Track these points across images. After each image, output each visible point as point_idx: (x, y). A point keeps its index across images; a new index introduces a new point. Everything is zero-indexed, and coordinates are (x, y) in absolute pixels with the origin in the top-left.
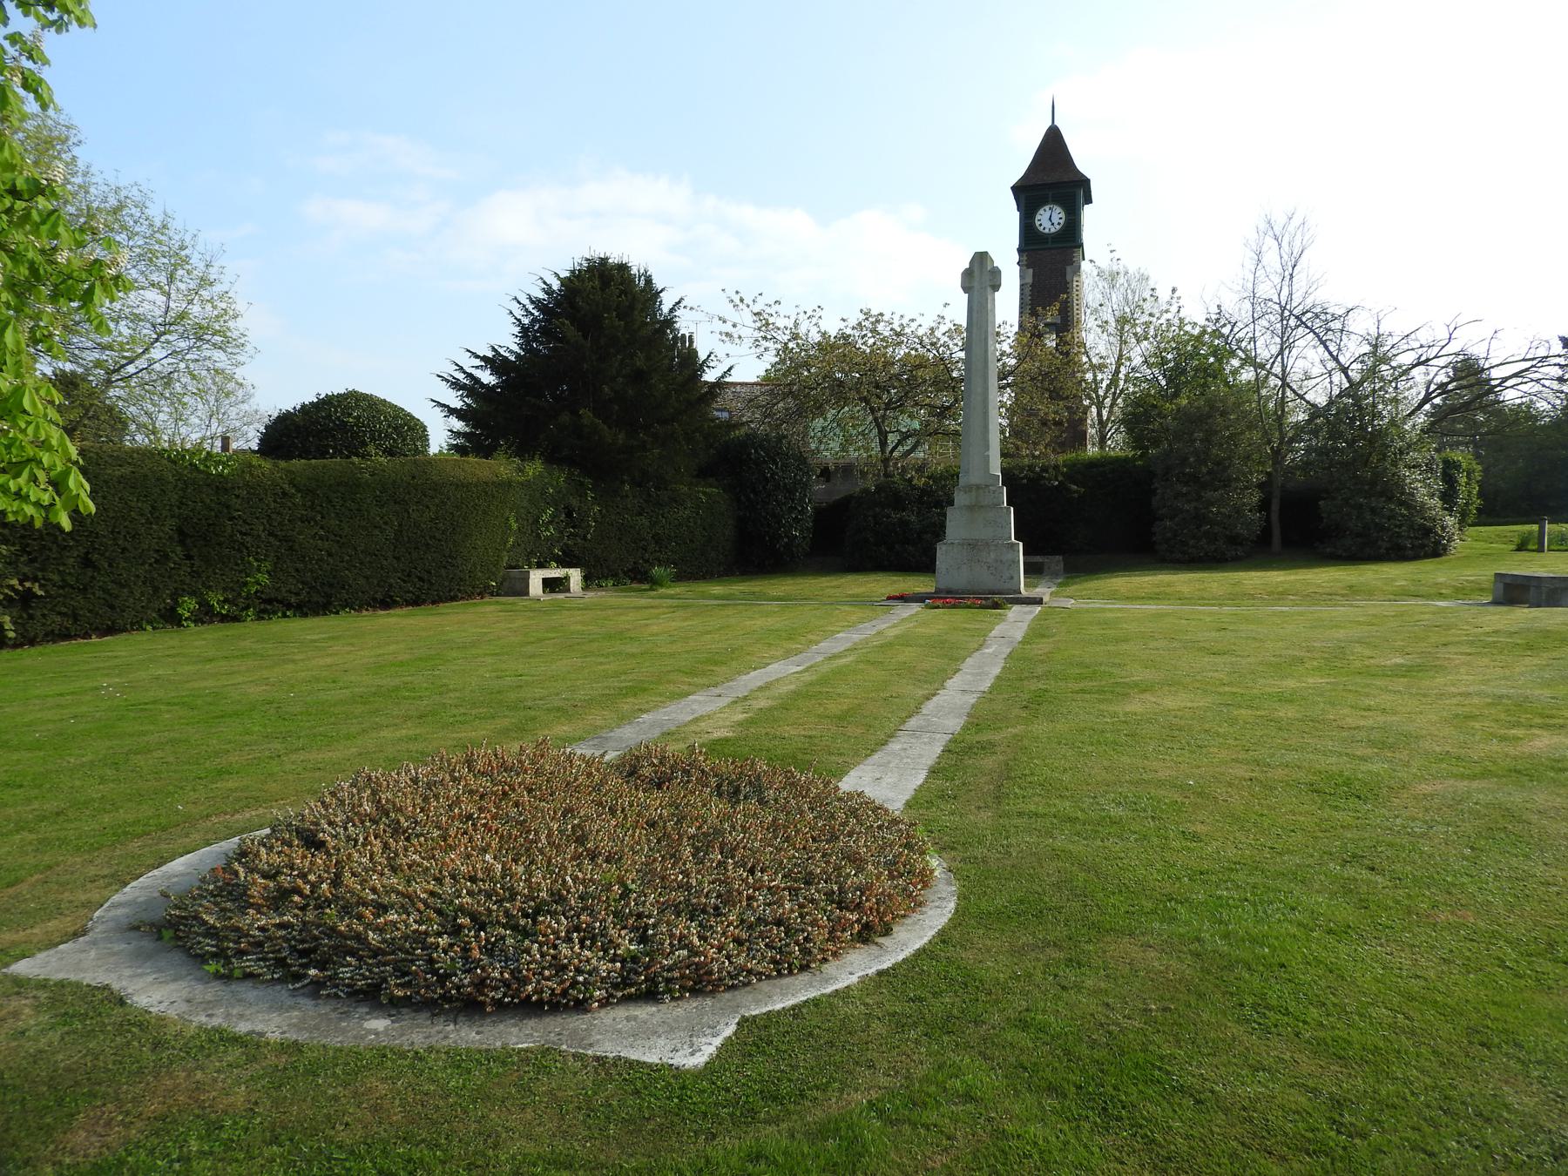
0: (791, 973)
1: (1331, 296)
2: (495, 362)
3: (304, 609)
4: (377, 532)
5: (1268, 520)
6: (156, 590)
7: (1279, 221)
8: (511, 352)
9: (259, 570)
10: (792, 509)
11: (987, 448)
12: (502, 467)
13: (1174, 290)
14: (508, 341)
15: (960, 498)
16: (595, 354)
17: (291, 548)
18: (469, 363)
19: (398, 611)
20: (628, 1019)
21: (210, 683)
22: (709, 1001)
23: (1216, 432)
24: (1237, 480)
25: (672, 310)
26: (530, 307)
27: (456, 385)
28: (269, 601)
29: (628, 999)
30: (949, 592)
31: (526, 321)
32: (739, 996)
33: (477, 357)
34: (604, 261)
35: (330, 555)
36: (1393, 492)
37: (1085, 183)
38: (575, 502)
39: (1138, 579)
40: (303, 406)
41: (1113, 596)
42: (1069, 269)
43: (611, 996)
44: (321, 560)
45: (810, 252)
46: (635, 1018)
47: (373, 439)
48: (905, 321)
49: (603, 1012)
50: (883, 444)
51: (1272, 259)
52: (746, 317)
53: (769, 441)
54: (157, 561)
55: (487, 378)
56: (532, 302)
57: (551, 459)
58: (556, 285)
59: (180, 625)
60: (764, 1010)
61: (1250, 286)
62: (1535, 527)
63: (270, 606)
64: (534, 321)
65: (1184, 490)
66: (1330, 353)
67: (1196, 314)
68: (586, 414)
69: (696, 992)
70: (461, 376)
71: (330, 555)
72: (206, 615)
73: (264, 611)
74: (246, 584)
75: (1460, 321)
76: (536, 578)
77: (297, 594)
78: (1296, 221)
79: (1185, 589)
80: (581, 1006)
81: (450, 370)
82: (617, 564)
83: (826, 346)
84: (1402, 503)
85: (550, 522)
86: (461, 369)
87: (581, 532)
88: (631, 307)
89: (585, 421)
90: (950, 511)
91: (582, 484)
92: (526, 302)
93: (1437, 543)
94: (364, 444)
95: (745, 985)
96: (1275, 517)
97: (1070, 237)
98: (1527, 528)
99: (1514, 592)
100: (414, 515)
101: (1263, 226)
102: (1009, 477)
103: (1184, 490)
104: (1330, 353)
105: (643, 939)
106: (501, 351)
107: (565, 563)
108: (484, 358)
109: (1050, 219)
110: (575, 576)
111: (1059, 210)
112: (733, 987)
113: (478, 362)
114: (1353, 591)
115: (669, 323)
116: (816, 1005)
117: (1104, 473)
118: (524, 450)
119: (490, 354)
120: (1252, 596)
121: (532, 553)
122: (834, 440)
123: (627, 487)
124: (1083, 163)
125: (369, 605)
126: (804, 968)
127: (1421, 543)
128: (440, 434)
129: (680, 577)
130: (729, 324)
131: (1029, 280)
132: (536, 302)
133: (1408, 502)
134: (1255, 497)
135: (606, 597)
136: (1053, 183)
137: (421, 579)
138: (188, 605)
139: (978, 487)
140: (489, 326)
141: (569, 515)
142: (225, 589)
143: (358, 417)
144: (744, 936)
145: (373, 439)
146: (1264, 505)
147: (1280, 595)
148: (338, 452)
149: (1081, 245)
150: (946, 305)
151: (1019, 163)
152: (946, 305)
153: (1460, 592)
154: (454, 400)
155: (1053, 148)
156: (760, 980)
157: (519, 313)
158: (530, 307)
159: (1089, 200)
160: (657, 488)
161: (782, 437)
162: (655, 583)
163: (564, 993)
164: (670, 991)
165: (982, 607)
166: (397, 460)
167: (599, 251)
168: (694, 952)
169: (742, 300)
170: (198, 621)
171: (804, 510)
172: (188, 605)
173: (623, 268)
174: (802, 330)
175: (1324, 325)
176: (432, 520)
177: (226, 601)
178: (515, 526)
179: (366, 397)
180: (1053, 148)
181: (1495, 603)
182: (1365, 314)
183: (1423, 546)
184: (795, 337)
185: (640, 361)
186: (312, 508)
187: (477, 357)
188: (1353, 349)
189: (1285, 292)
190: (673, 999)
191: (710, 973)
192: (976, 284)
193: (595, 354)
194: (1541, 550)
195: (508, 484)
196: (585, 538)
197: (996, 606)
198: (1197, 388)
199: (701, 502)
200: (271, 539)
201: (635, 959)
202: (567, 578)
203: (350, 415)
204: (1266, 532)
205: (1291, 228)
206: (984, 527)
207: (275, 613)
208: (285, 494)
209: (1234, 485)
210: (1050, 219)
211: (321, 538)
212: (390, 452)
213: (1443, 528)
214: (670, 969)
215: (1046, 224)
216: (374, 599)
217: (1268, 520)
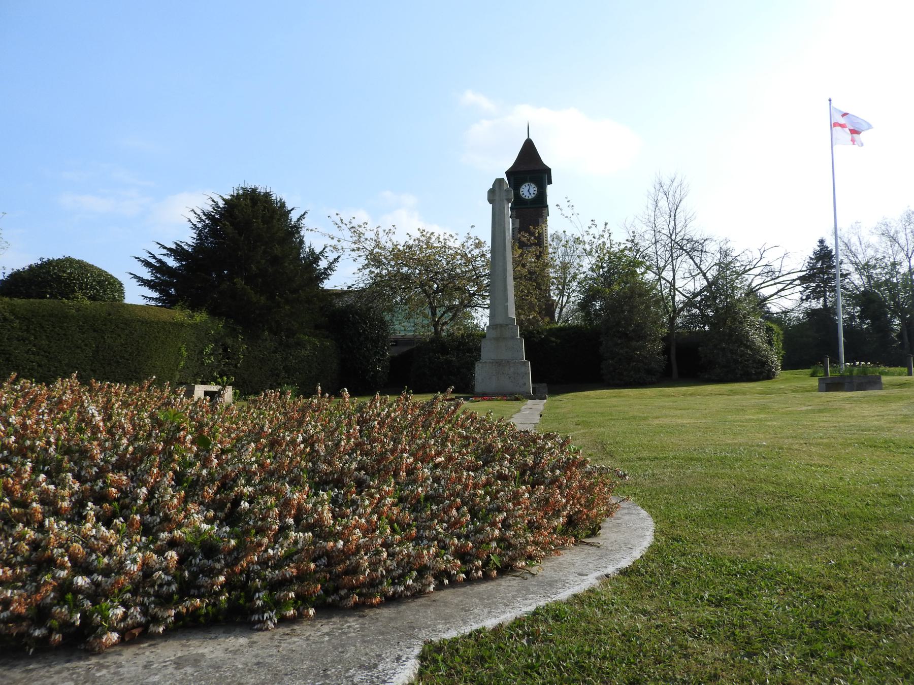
0: (486, 578)
1: (695, 231)
2: (178, 252)
4: (79, 351)
5: (669, 360)
7: (666, 182)
8: (190, 246)
10: (376, 353)
11: (506, 300)
12: (179, 315)
13: (606, 224)
14: (188, 238)
16: (245, 256)
17: (8, 360)
18: (158, 252)
20: (179, 663)
22: (353, 623)
23: (636, 307)
24: (651, 335)
25: (299, 219)
26: (204, 218)
27: (147, 264)
29: (190, 625)
31: (199, 225)
32: (409, 611)
33: (165, 248)
34: (254, 190)
35: (39, 366)
36: (742, 340)
37: (548, 171)
38: (229, 341)
40: (30, 266)
42: (540, 220)
43: (156, 620)
44: (32, 369)
46: (196, 661)
47: (81, 288)
49: (128, 653)
50: (434, 314)
51: (663, 204)
52: (347, 234)
53: (361, 310)
55: (171, 262)
56: (205, 214)
57: (214, 312)
58: (221, 204)
60: (467, 630)
61: (652, 219)
64: (205, 226)
65: (619, 341)
66: (696, 264)
67: (619, 239)
68: (239, 282)
69: (327, 609)
70: (153, 261)
71: (39, 366)
75: (767, 247)
78: (675, 184)
80: (80, 641)
84: (747, 347)
85: (211, 354)
86: (154, 257)
87: (233, 362)
88: (272, 217)
89: (238, 286)
91: (234, 330)
92: (201, 214)
93: (770, 371)
94: (73, 291)
95: (418, 594)
96: (673, 358)
97: (540, 203)
100: (109, 341)
101: (658, 187)
103: (619, 341)
104: (696, 264)
105: (230, 515)
106: (182, 245)
108: (169, 249)
109: (528, 191)
111: (533, 186)
112: (391, 600)
113: (165, 251)
115: (297, 228)
116: (556, 618)
117: (568, 333)
118: (194, 306)
119: (174, 247)
121: (197, 375)
123: (266, 333)
124: (547, 160)
126: (506, 570)
128: (136, 295)
130: (336, 239)
131: (517, 226)
132: (208, 215)
133: (750, 345)
136: (529, 170)
139: (501, 326)
140: (177, 222)
141: (225, 350)
144: (408, 517)
145: (81, 288)
146: (666, 351)
148: (53, 296)
149: (547, 206)
154: (146, 274)
155: (529, 151)
156: (440, 587)
157: (195, 220)
158: (204, 218)
159: (550, 182)
160: (287, 337)
161: (369, 309)
163: (41, 614)
164: (277, 605)
166: (98, 303)
167: (251, 184)
168: (318, 530)
171: (384, 355)
173: (267, 195)
174: (383, 242)
175: (692, 248)
176: (122, 345)
178: (185, 354)
179: (79, 262)
180: (529, 151)
182: (713, 243)
183: (761, 373)
184: (378, 245)
185: (277, 250)
186: (27, 330)
187: (165, 248)
188: (709, 261)
190: (283, 621)
191: (355, 570)
192: (497, 198)
193: (245, 256)
195: (182, 325)
196: (236, 366)
197: (517, 399)
198: (620, 284)
199: (313, 345)
201: (210, 549)
203: (64, 272)
204: (669, 366)
205: (673, 188)
208: (5, 319)
209: (648, 338)
210: (528, 191)
211: (33, 354)
212: (93, 298)
213: (772, 362)
214: (279, 564)
217: (669, 360)
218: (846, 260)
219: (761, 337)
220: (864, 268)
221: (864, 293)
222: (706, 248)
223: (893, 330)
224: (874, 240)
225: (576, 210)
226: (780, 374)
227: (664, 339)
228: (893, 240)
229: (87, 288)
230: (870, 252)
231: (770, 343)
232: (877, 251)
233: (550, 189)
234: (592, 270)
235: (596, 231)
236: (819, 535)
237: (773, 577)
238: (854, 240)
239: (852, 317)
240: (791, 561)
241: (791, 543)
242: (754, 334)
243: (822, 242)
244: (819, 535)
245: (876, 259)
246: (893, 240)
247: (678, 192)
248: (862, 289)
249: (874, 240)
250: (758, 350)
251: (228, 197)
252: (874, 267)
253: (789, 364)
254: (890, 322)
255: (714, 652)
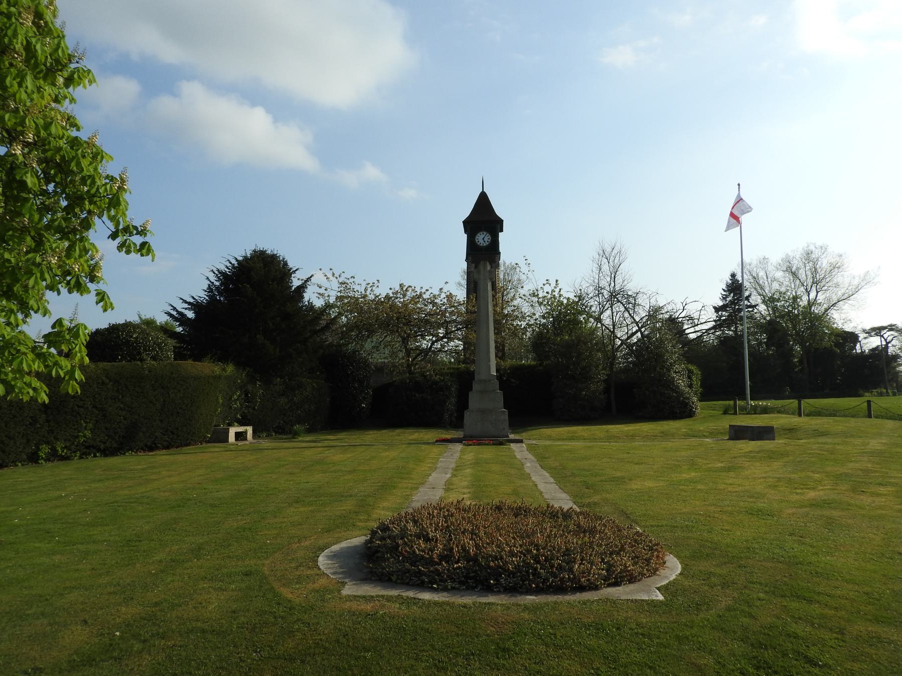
1: (631, 287)
2: (195, 306)
3: (107, 452)
6: (28, 441)
9: (85, 429)
15: (476, 386)
17: (104, 416)
18: (180, 306)
19: (158, 452)
21: (126, 492)
28: (88, 447)
30: (471, 437)
35: (125, 419)
38: (250, 387)
39: (560, 429)
41: (550, 438)
45: (378, 251)
47: (145, 350)
48: (423, 291)
54: (30, 424)
55: (190, 315)
57: (239, 364)
59: (36, 462)
61: (596, 281)
62: (732, 403)
63: (89, 450)
67: (568, 293)
70: (174, 313)
71: (125, 419)
72: (54, 456)
73: (84, 454)
74: (77, 437)
76: (232, 431)
77: (104, 443)
78: (615, 251)
79: (585, 434)
81: (169, 309)
82: (272, 424)
83: (378, 302)
86: (175, 309)
90: (471, 395)
97: (493, 251)
98: (727, 402)
99: (738, 433)
101: (601, 252)
102: (499, 377)
107: (242, 424)
108: (189, 303)
109: (483, 239)
110: (250, 429)
113: (186, 306)
114: (665, 435)
118: (223, 358)
119: (192, 300)
120: (619, 438)
122: (378, 352)
124: (499, 211)
125: (142, 449)
127: (683, 411)
129: (310, 431)
130: (323, 288)
133: (676, 389)
134: (602, 387)
135: (265, 443)
136: (483, 222)
137: (173, 433)
138: (45, 450)
141: (246, 395)
142: (65, 440)
143: (137, 338)
146: (607, 391)
147: (632, 437)
150: (446, 283)
151: (466, 212)
152: (446, 283)
153: (712, 434)
155: (483, 202)
162: (295, 434)
165: (493, 444)
167: (261, 247)
169: (333, 274)
170: (48, 460)
172: (45, 450)
175: (629, 301)
177: (66, 447)
180: (483, 202)
181: (730, 439)
189: (613, 285)
194: (735, 413)
196: (254, 409)
200: (94, 409)
202: (246, 432)
206: (487, 402)
207: (90, 454)
208: (103, 383)
210: (483, 239)
212: (154, 358)
215: (482, 241)
216: (146, 446)
218: (754, 293)
219: (683, 381)
220: (770, 301)
221: (770, 323)
222: (639, 301)
223: (794, 356)
224: (779, 274)
225: (532, 268)
226: (700, 407)
227: (605, 381)
228: (794, 275)
229: (149, 350)
230: (775, 286)
231: (690, 386)
232: (781, 284)
233: (503, 238)
234: (543, 317)
235: (548, 288)
236: (725, 563)
237: (714, 575)
238: (762, 274)
239: (760, 343)
240: (718, 571)
241: (717, 566)
242: (679, 379)
243: (733, 275)
244: (725, 563)
245: (780, 293)
246: (794, 275)
247: (617, 258)
248: (768, 318)
249: (779, 274)
250: (680, 394)
251: (240, 259)
252: (778, 300)
253: (708, 394)
254: (792, 349)
255: (706, 588)
